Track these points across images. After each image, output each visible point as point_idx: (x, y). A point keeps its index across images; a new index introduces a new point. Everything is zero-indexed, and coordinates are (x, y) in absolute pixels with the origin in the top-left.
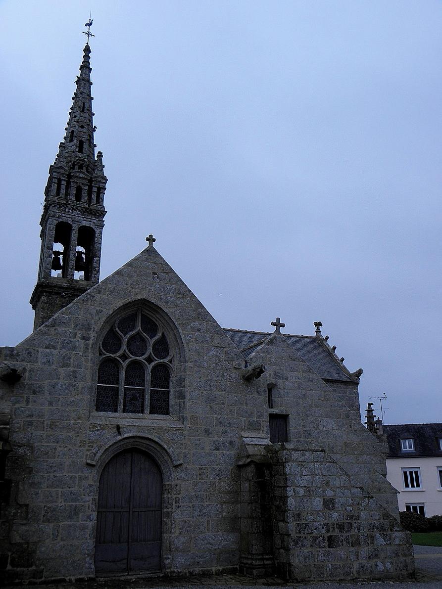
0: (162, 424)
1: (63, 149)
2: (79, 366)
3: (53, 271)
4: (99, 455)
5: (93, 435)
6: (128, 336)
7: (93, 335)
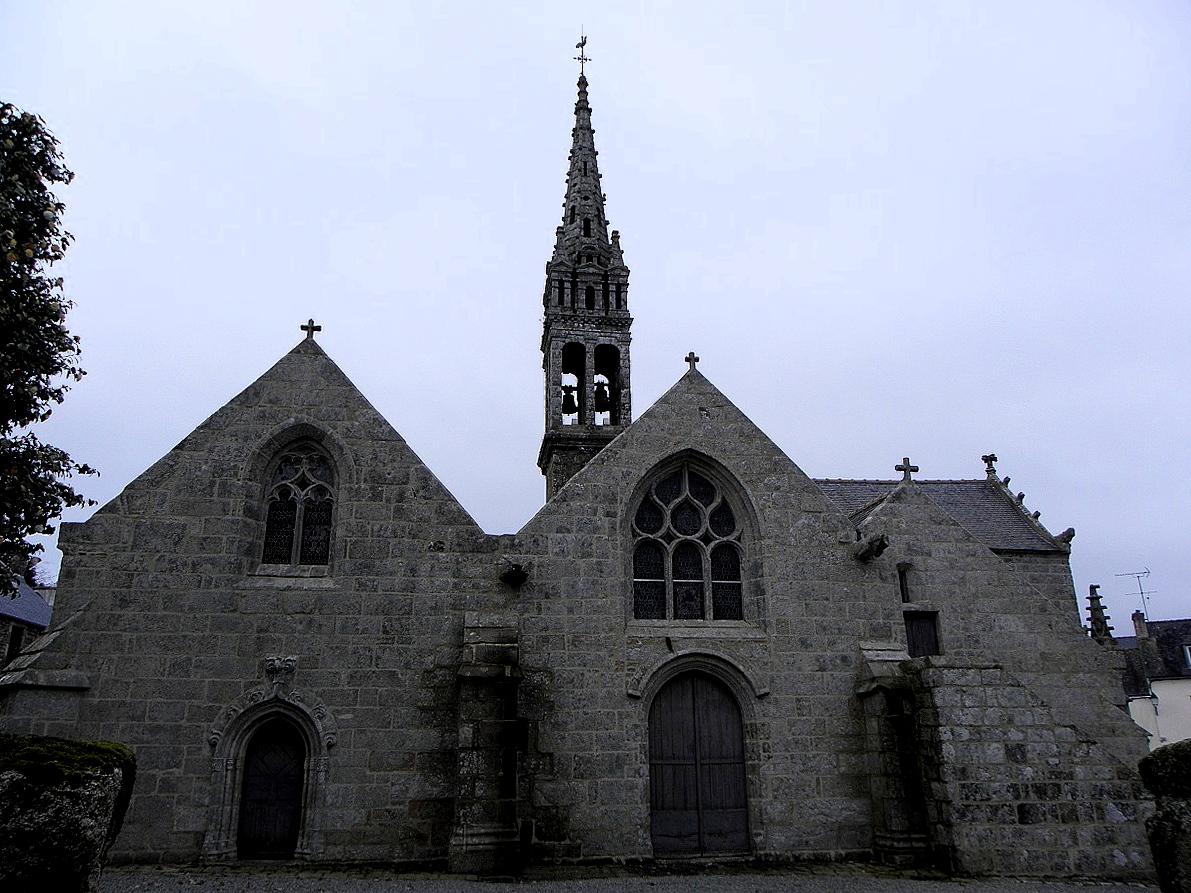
0: (733, 634)
1: (562, 235)
2: (604, 555)
3: (565, 416)
4: (645, 681)
5: (634, 653)
6: (672, 506)
7: (620, 509)
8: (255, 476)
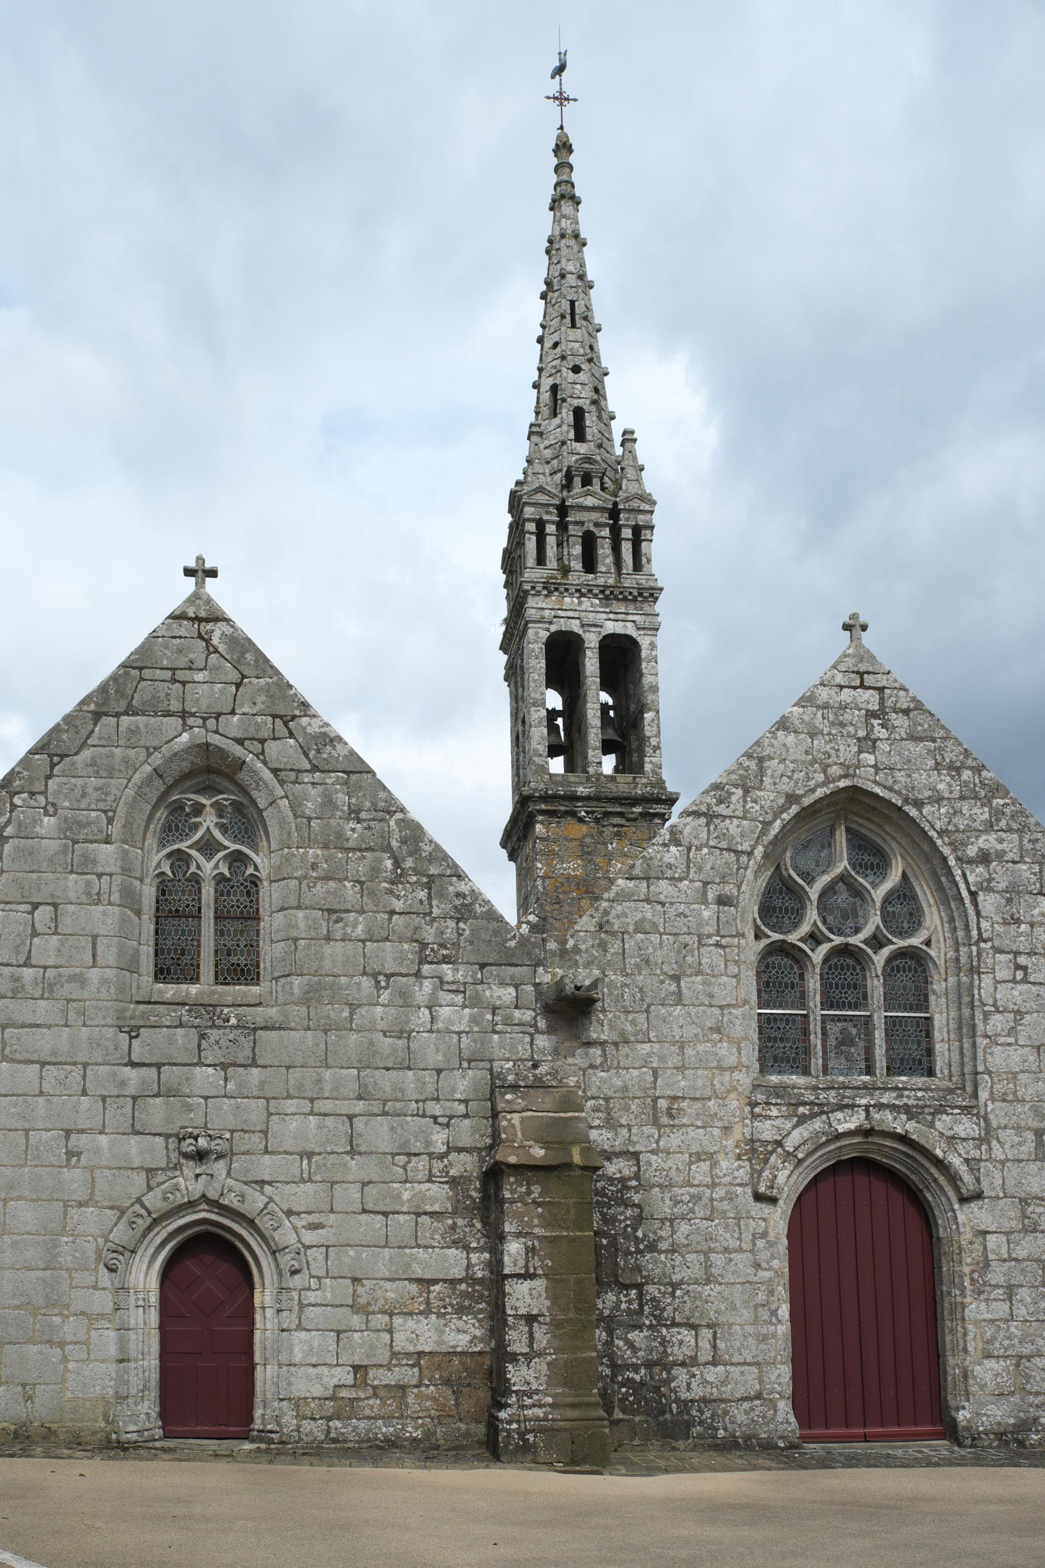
8: (133, 836)
